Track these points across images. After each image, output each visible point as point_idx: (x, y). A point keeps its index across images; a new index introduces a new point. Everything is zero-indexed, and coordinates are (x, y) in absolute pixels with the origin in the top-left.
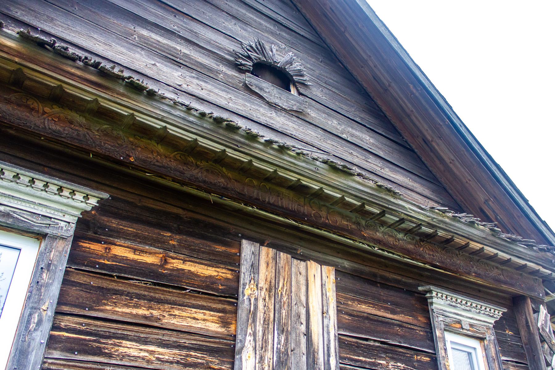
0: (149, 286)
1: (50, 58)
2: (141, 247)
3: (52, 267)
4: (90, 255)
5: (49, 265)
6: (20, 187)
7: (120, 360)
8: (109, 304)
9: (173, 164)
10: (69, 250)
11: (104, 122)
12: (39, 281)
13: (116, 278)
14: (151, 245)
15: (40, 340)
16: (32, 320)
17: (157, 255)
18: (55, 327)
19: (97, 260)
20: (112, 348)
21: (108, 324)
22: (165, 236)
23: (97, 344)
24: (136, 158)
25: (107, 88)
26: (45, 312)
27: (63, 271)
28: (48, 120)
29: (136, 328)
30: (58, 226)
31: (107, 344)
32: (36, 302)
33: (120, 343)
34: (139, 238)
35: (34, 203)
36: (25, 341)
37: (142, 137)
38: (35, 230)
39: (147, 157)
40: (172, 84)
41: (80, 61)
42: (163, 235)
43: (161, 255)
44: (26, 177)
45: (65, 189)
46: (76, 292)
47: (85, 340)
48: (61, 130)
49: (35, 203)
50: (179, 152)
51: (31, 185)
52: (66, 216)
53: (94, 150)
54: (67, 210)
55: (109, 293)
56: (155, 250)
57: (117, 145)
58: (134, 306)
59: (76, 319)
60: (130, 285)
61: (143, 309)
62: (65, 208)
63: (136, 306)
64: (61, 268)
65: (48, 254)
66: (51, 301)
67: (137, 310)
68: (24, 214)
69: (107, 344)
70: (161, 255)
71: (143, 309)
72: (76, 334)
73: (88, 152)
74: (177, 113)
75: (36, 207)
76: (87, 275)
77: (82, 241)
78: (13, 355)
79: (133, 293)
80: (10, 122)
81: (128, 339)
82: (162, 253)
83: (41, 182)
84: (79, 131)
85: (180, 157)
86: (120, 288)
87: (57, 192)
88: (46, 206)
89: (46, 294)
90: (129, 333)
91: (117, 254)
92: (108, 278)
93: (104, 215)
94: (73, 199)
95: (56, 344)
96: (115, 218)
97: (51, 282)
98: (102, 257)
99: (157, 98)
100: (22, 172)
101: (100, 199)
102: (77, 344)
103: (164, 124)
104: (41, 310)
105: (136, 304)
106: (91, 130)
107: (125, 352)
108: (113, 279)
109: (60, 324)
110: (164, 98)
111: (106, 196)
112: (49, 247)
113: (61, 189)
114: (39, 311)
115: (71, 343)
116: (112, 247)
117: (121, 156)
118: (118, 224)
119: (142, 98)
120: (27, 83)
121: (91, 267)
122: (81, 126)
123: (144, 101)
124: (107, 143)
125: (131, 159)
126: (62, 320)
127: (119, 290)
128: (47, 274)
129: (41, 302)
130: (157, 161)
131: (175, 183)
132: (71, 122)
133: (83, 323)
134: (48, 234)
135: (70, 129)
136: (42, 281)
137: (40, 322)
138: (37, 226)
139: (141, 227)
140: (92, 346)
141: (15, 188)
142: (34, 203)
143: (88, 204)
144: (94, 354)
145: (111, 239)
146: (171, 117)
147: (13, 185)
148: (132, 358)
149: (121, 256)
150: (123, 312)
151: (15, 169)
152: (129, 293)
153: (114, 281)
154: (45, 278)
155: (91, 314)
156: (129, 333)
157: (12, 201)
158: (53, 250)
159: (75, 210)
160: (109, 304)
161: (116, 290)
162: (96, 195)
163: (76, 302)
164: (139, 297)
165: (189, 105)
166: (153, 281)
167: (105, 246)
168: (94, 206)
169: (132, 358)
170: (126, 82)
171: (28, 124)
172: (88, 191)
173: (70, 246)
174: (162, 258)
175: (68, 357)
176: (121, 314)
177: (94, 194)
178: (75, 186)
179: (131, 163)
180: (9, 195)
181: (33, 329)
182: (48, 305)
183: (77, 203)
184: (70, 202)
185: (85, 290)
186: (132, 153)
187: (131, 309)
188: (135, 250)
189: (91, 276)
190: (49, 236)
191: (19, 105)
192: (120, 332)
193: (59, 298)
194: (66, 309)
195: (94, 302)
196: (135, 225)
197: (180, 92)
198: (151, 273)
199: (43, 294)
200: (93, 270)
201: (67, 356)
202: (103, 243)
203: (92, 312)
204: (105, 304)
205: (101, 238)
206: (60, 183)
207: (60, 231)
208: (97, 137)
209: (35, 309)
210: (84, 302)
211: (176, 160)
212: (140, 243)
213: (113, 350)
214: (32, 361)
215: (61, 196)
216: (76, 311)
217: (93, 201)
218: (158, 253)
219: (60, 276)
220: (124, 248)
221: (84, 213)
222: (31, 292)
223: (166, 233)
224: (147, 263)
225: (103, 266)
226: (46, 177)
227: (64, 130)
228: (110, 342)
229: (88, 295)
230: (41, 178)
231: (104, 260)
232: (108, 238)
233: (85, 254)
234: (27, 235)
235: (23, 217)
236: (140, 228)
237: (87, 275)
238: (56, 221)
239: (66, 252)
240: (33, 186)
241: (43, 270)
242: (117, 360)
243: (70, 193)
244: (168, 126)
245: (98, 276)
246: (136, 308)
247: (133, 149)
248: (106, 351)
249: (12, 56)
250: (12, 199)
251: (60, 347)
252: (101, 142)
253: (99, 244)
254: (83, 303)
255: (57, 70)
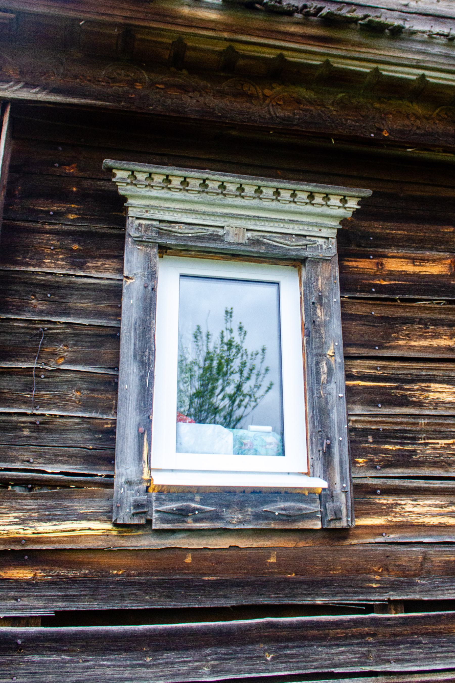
0: (443, 306)
1: (262, 20)
2: (419, 254)
3: (324, 300)
4: (360, 277)
5: (320, 298)
6: (264, 203)
7: (434, 409)
8: (401, 337)
9: (440, 127)
10: (337, 274)
11: (339, 90)
12: (314, 320)
13: (399, 301)
14: (431, 249)
15: (337, 393)
16: (322, 370)
17: (443, 262)
18: (349, 377)
19: (371, 282)
20: (420, 394)
21: (407, 364)
22: (446, 233)
23: (402, 392)
24: (390, 130)
25: (337, 41)
26: (333, 358)
27: (338, 304)
28: (273, 105)
29: (442, 366)
30: (316, 245)
31: (412, 390)
32: (319, 348)
33: (428, 387)
34: (414, 241)
35: (283, 221)
36: (321, 397)
37: (389, 99)
38: (292, 255)
39: (404, 126)
40: (395, 7)
41: (298, 13)
42: (443, 232)
43: (449, 261)
44: (269, 189)
45: (316, 195)
46: (358, 328)
47: (385, 388)
48: (291, 115)
49: (284, 220)
50: (442, 107)
51: (277, 198)
52: (323, 230)
53: (335, 132)
54: (322, 222)
55: (397, 324)
56: (439, 255)
57: (361, 118)
58: (432, 335)
59: (368, 362)
60: (420, 308)
61: (445, 339)
62: (319, 220)
63: (436, 336)
64: (335, 300)
65: (315, 284)
66: (337, 344)
67: (436, 340)
68: (275, 237)
69: (412, 390)
70: (449, 261)
71: (445, 339)
72: (373, 381)
73: (327, 137)
74: (436, 50)
75: (286, 226)
76: (366, 303)
77: (346, 259)
78: (311, 415)
79: (426, 319)
80: (233, 120)
81: (436, 380)
82: (449, 258)
83: (287, 191)
84: (311, 111)
85: (446, 114)
86: (409, 315)
87: (308, 201)
88: (297, 222)
89: (327, 335)
90: (435, 373)
91: (393, 269)
92: (390, 303)
93: (362, 220)
94: (329, 206)
95: (354, 396)
96: (377, 220)
97: (328, 319)
98: (375, 276)
99: (403, 35)
100: (265, 183)
101: (360, 199)
102: (377, 394)
103: (421, 72)
104: (328, 356)
105: (433, 333)
106: (324, 106)
107: (437, 399)
108: (396, 304)
109: (351, 371)
110: (415, 33)
111: (368, 193)
112: (313, 275)
113: (311, 196)
114: (325, 358)
115: (370, 393)
116: (384, 261)
117: (372, 133)
118: (382, 228)
119: (383, 42)
120: (241, 62)
121: (366, 292)
122: (311, 103)
123: (390, 46)
124: (349, 119)
125: (384, 133)
126: (352, 365)
127: (407, 318)
128: (321, 310)
129: (324, 345)
130: (418, 128)
131: (448, 154)
132: (298, 101)
133: (377, 367)
134: (307, 258)
135: (301, 112)
136: (318, 319)
137: (330, 372)
138: (294, 250)
139: (413, 226)
140: (395, 395)
141: (259, 205)
142: (283, 221)
143: (348, 209)
144: (401, 405)
145: (381, 250)
146: (428, 58)
147: (256, 201)
148: (448, 405)
149: (398, 271)
150: (421, 346)
151: (256, 182)
152: (421, 319)
153: (399, 306)
154: (320, 315)
155: (384, 353)
156: (435, 373)
157: (258, 223)
158: (320, 278)
159: (332, 219)
160: (401, 337)
161: (404, 318)
162: (356, 194)
163: (361, 341)
164: (436, 323)
165: (449, 33)
166: (447, 298)
167: (375, 261)
168: (355, 210)
169: (448, 405)
170: (360, 24)
171: (253, 118)
172: (310, 188)
173: (337, 269)
174: (450, 264)
175: (372, 411)
176: (419, 348)
177: (353, 194)
178: (328, 187)
179: (386, 139)
180: (254, 217)
181: (325, 381)
182: (334, 349)
183: (334, 210)
184: (325, 210)
185: (367, 323)
186: (383, 125)
187: (429, 340)
188: (413, 260)
189: (369, 304)
190: (309, 261)
191: (235, 95)
192: (424, 373)
193: (344, 340)
194: (353, 351)
195: (383, 338)
196: (404, 226)
197: (409, 15)
198: (443, 287)
199: (324, 336)
200: (370, 296)
201: (370, 411)
202: (371, 257)
203: (384, 351)
204: (397, 339)
205: (367, 251)
206: (310, 188)
207: (320, 251)
208: (334, 113)
209: (320, 356)
210: (371, 339)
211: (441, 120)
212: (417, 248)
213: (421, 398)
214: (336, 421)
215: (313, 204)
216: (365, 352)
217: (353, 204)
218: (444, 259)
219: (336, 310)
220: (398, 260)
221: (343, 221)
222: (308, 335)
223: (447, 229)
224: (432, 275)
225: (381, 289)
226: (293, 184)
227: (294, 114)
228: (415, 387)
229: (373, 330)
230: (287, 185)
231: (379, 280)
232: (376, 249)
233: (355, 276)
234: (281, 263)
235: (275, 241)
236: (412, 228)
237: (366, 303)
238: (313, 239)
239: (335, 278)
240: (243, 194)
241: (316, 305)
242: (430, 409)
243: (324, 198)
244: (427, 73)
245: (378, 302)
246: (436, 339)
247: (383, 119)
248: (414, 399)
249: (219, 33)
250: (258, 220)
251: (359, 400)
252: (341, 119)
253: (368, 260)
254: (370, 341)
255: (274, 34)
